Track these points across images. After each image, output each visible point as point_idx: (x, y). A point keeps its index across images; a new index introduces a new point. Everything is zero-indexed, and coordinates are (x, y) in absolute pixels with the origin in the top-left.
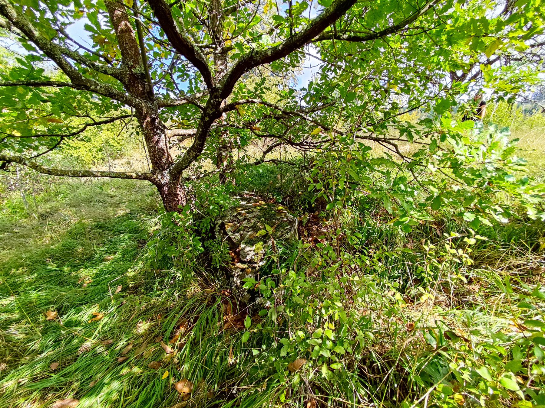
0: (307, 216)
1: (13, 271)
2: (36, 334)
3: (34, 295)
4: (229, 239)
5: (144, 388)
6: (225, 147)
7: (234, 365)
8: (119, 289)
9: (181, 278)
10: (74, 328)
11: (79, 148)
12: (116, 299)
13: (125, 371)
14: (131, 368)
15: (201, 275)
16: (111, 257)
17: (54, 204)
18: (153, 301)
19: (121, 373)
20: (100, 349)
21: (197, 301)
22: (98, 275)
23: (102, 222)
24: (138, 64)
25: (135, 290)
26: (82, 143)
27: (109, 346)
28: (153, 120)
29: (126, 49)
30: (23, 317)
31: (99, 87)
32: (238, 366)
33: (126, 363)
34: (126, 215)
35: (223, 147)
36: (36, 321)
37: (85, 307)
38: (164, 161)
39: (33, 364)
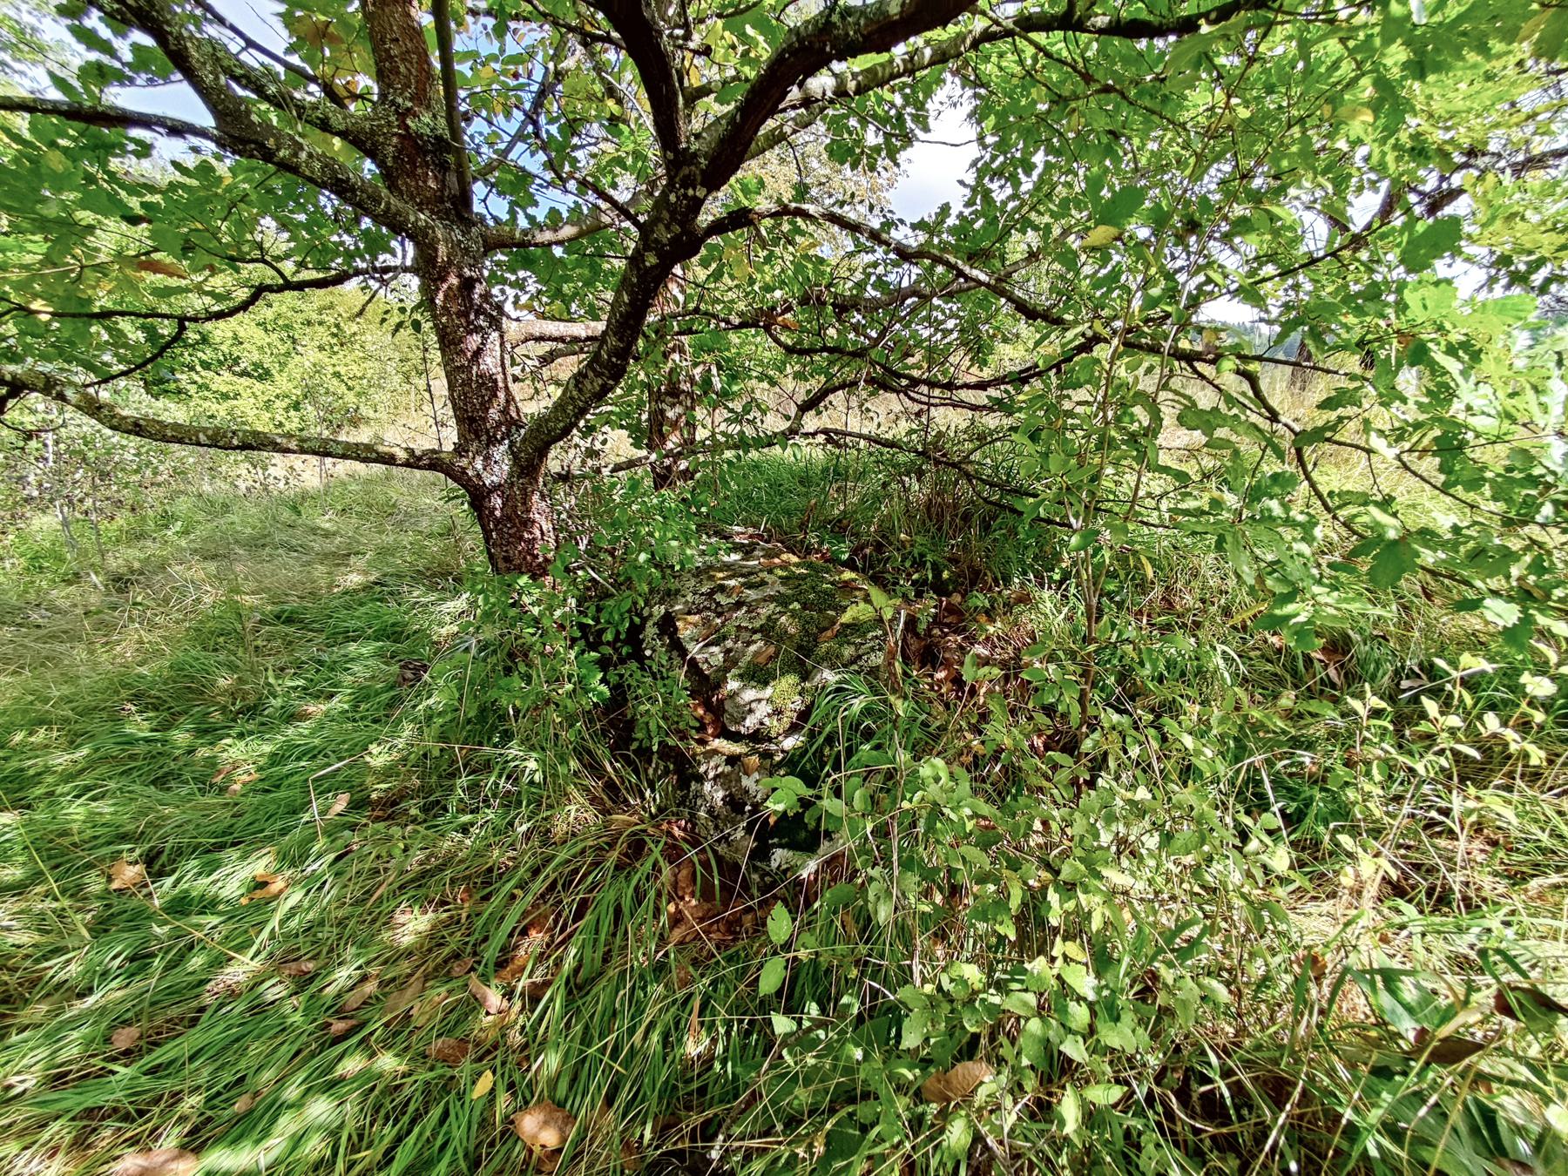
0: (928, 607)
1: (19, 737)
2: (72, 932)
3: (76, 812)
4: (693, 663)
5: (413, 1122)
6: (674, 392)
7: (707, 1061)
8: (341, 804)
9: (538, 777)
10: (195, 919)
11: (237, 395)
12: (332, 832)
13: (352, 1065)
14: (373, 1055)
15: (595, 769)
16: (317, 708)
17: (152, 548)
18: (447, 844)
19: (339, 1070)
20: (273, 991)
21: (583, 851)
22: (275, 759)
23: (293, 603)
24: (428, 107)
25: (389, 808)
26: (245, 381)
27: (303, 982)
28: (468, 285)
29: (391, 58)
30: (37, 877)
31: (303, 155)
32: (717, 1066)
33: (355, 1040)
34: (367, 588)
35: (667, 393)
36: (77, 893)
37: (233, 853)
38: (494, 414)
39: (58, 1030)
